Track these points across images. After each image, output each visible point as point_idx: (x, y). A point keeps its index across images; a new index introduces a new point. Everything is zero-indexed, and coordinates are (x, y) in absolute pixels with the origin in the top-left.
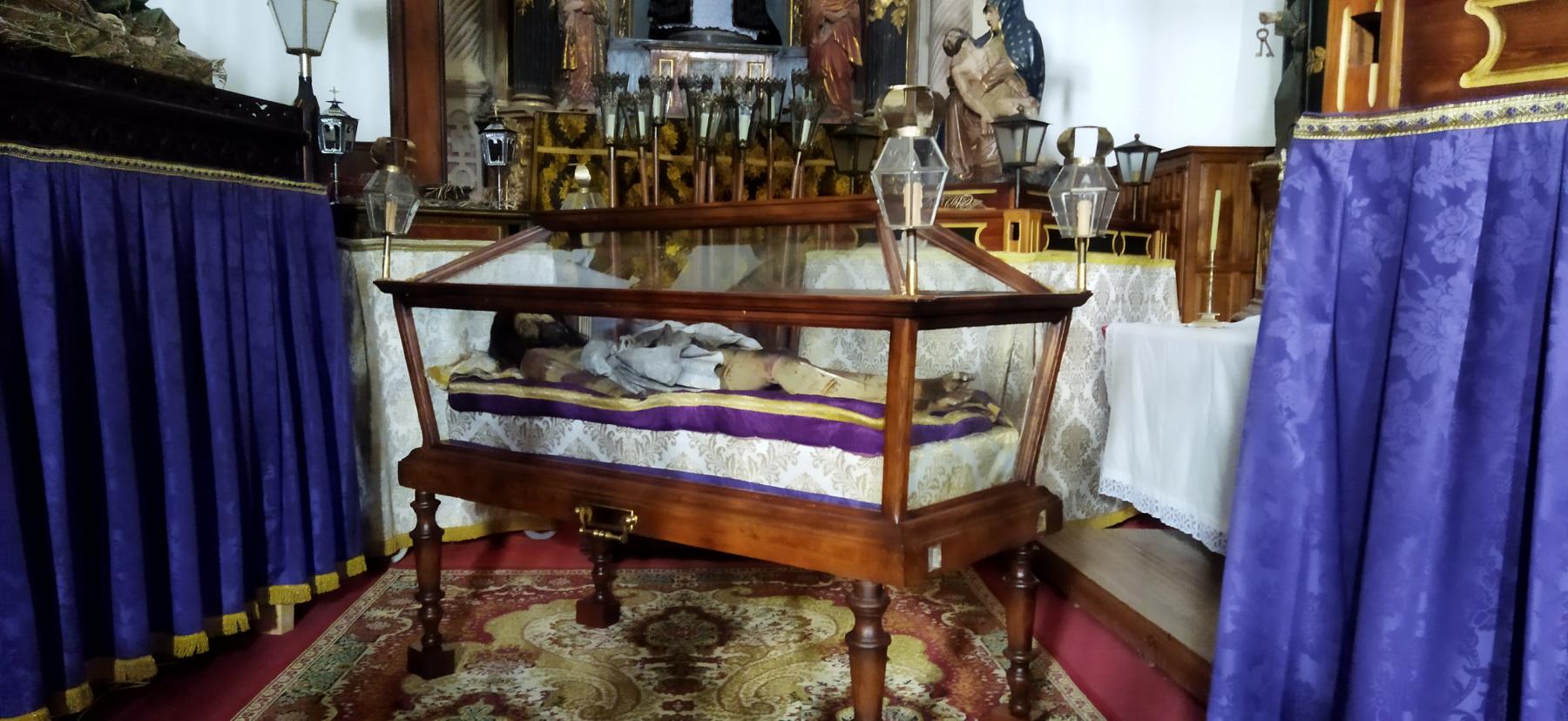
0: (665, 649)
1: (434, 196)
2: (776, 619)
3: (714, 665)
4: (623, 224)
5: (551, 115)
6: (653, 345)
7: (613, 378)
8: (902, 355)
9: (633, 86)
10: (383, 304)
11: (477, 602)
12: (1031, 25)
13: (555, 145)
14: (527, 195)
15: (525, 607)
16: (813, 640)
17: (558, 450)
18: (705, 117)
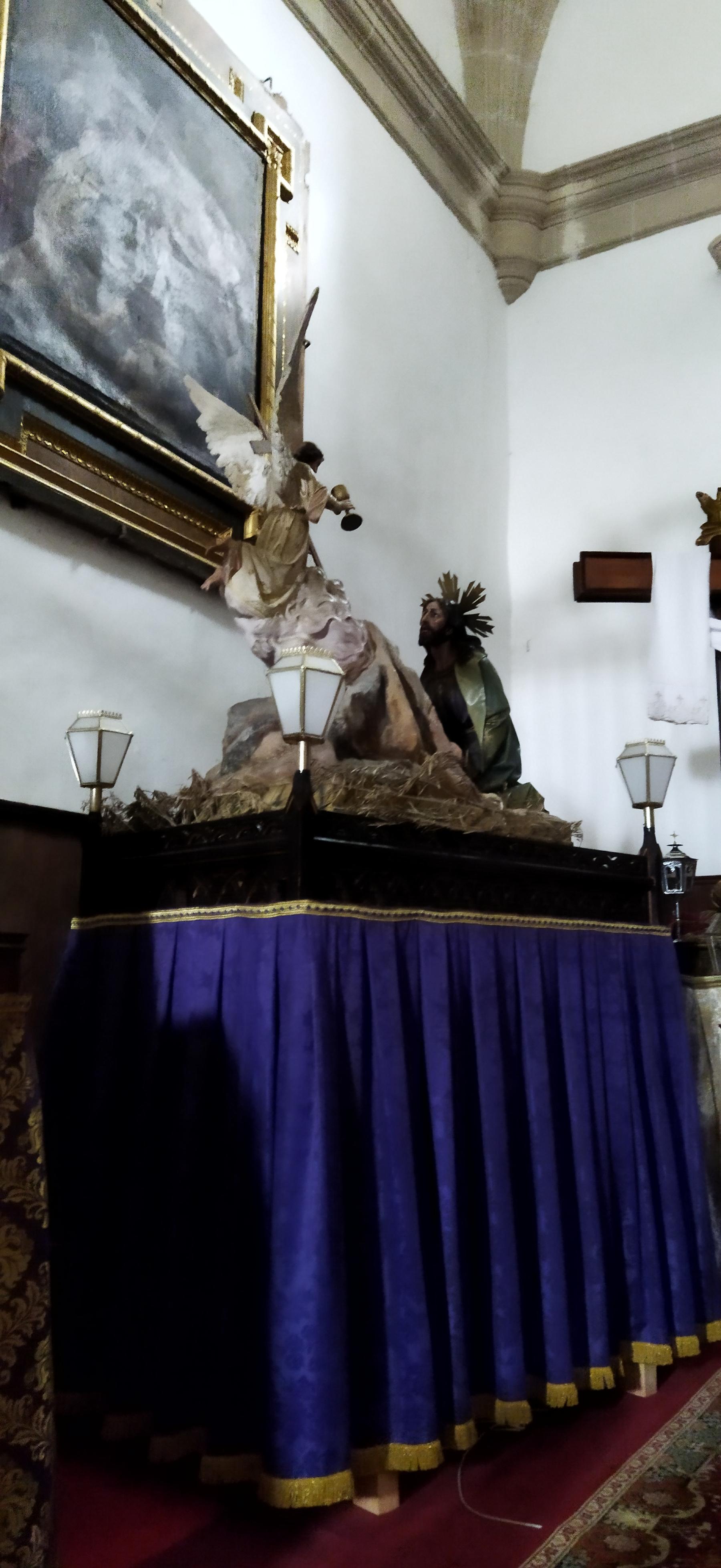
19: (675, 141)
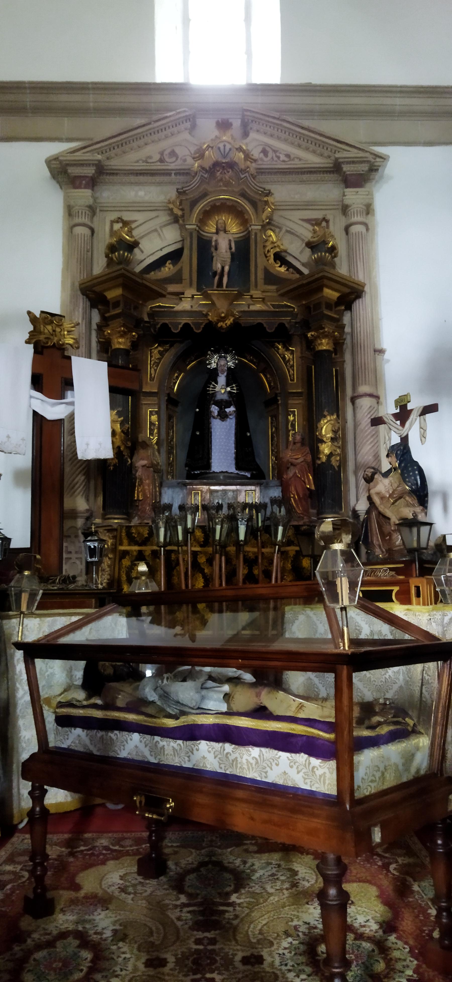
0: (198, 895)
1: (54, 582)
2: (274, 870)
3: (231, 909)
4: (167, 603)
5: (127, 527)
6: (184, 680)
7: (159, 703)
8: (343, 689)
9: (175, 510)
10: (19, 655)
11: (71, 859)
12: (416, 463)
13: (129, 545)
14: (112, 576)
15: (103, 863)
16: (300, 889)
17: (123, 754)
18: (218, 527)
19: (30, 88)
